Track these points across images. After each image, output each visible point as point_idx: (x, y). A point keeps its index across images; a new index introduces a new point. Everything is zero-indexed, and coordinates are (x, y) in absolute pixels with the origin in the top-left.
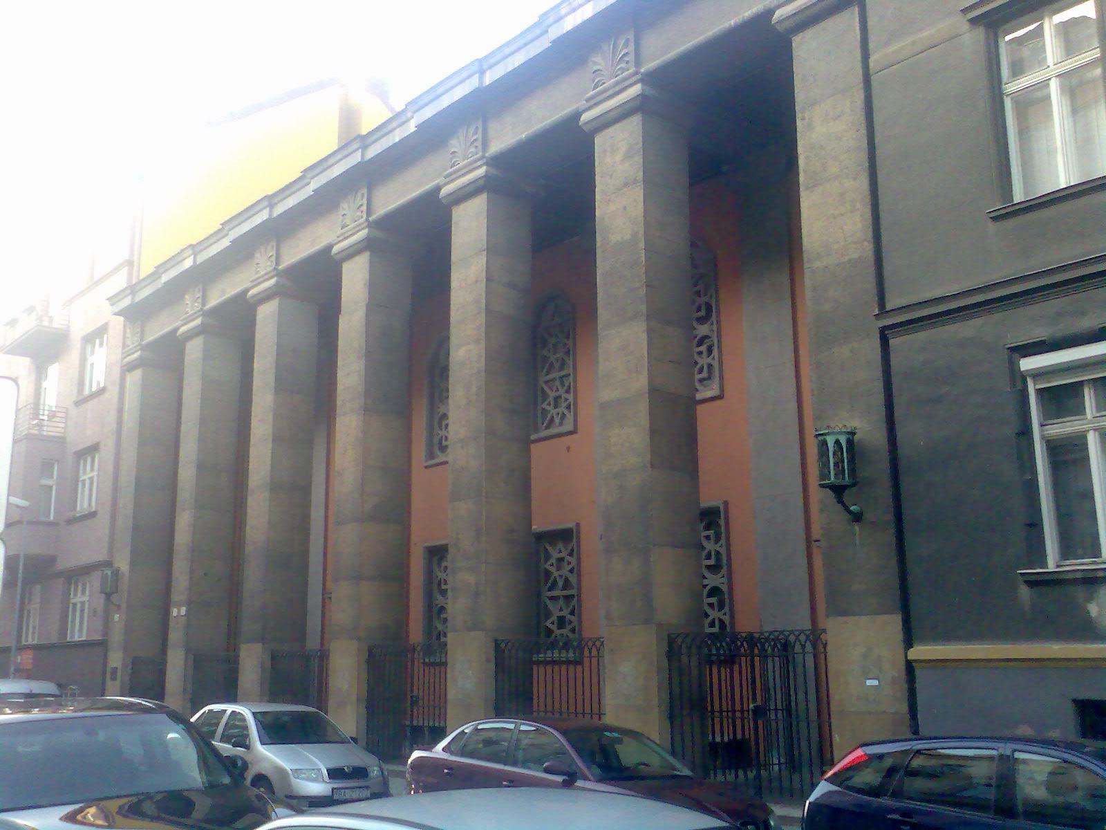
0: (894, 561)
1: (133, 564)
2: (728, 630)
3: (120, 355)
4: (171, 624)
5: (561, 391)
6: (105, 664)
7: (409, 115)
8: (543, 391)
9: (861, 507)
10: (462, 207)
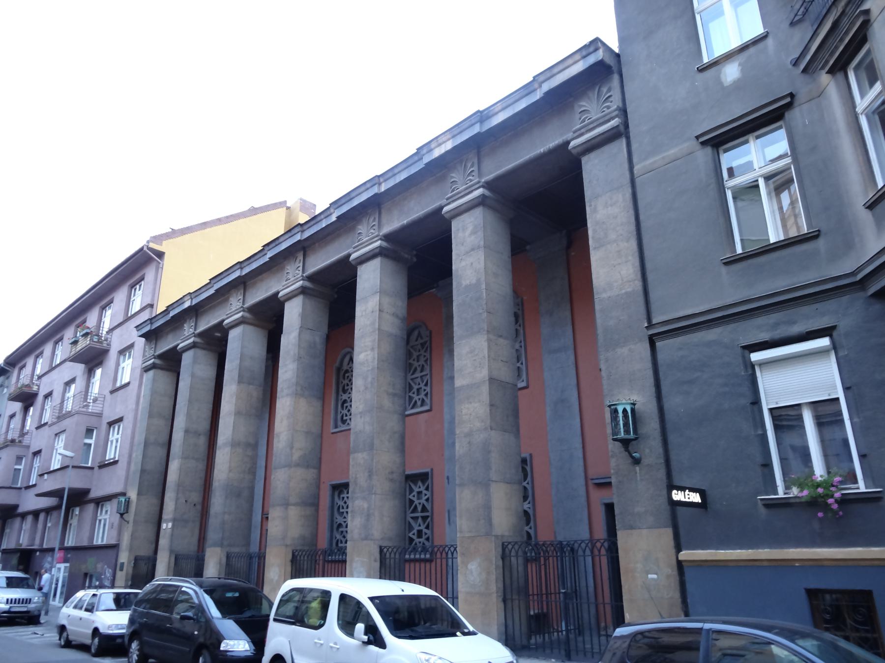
2: (533, 539)
5: (422, 385)
6: (116, 560)
7: (332, 210)
9: (640, 454)
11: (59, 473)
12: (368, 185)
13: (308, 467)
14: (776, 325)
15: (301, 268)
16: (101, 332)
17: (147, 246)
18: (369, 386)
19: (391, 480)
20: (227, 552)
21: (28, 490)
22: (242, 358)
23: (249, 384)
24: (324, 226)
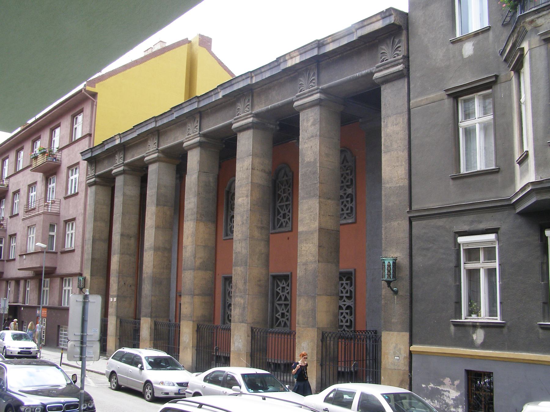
0: (408, 312)
1: (92, 275)
3: (85, 179)
4: (110, 305)
5: (286, 211)
7: (219, 90)
8: (278, 210)
10: (242, 134)
11: (34, 256)
12: (244, 77)
13: (206, 270)
14: (472, 222)
15: (198, 127)
16: (52, 149)
17: (85, 89)
18: (245, 222)
19: (259, 286)
20: (155, 321)
21: (9, 263)
22: (159, 187)
23: (164, 205)
24: (214, 100)
